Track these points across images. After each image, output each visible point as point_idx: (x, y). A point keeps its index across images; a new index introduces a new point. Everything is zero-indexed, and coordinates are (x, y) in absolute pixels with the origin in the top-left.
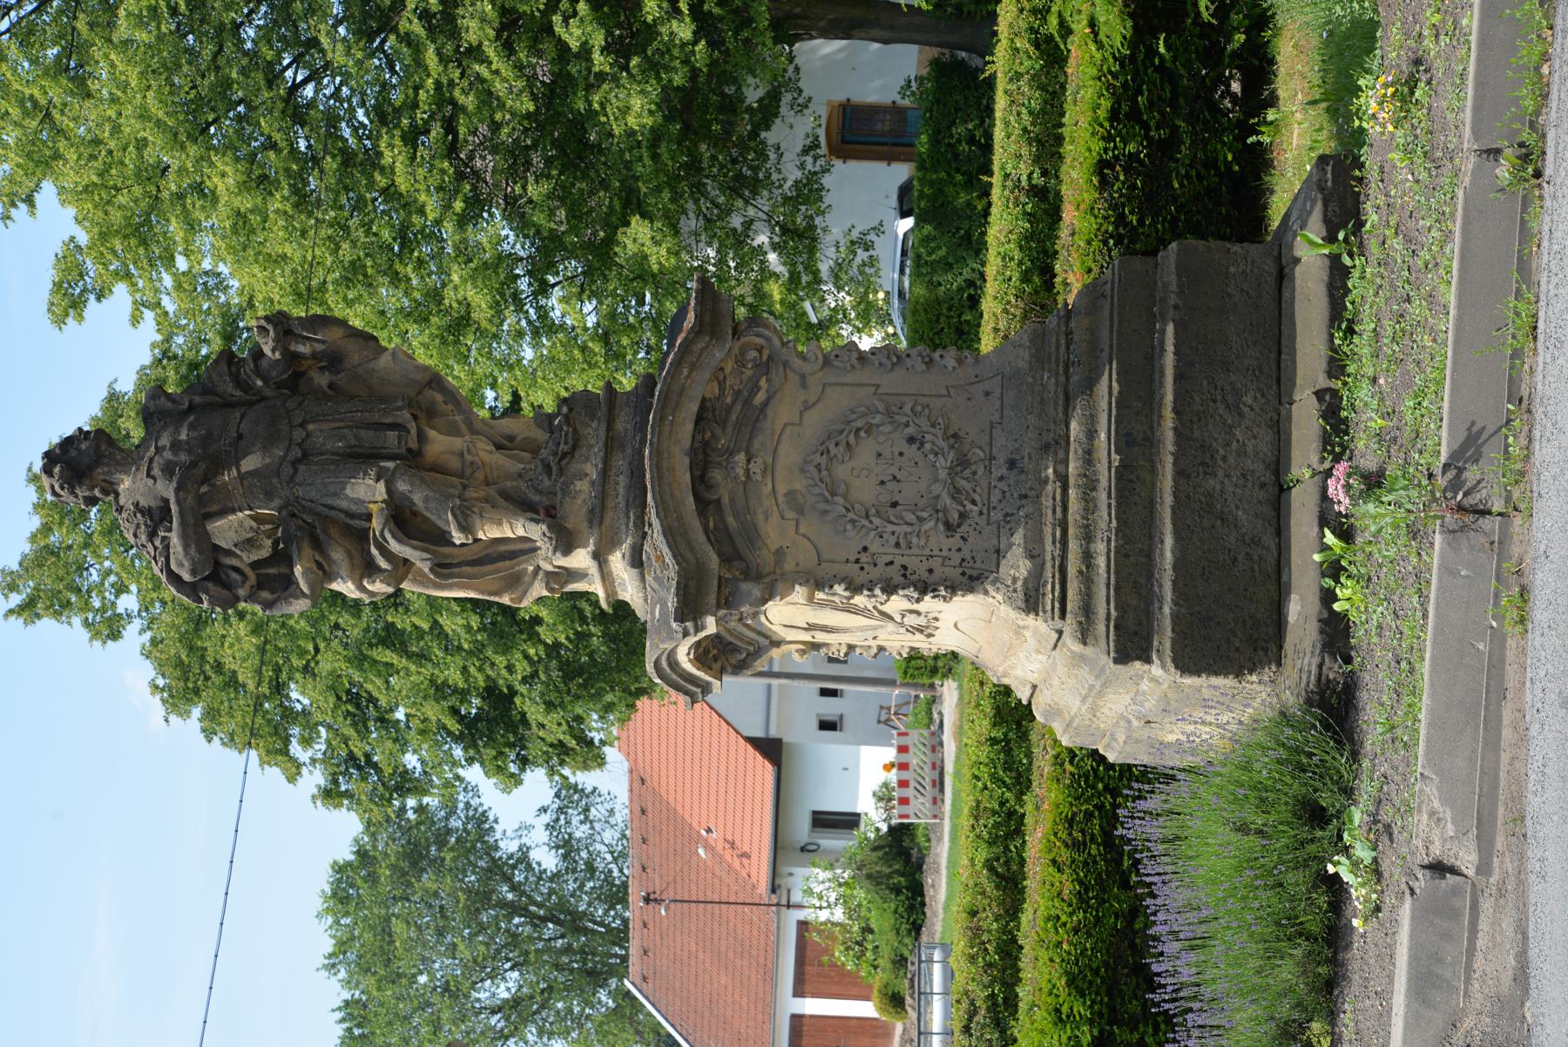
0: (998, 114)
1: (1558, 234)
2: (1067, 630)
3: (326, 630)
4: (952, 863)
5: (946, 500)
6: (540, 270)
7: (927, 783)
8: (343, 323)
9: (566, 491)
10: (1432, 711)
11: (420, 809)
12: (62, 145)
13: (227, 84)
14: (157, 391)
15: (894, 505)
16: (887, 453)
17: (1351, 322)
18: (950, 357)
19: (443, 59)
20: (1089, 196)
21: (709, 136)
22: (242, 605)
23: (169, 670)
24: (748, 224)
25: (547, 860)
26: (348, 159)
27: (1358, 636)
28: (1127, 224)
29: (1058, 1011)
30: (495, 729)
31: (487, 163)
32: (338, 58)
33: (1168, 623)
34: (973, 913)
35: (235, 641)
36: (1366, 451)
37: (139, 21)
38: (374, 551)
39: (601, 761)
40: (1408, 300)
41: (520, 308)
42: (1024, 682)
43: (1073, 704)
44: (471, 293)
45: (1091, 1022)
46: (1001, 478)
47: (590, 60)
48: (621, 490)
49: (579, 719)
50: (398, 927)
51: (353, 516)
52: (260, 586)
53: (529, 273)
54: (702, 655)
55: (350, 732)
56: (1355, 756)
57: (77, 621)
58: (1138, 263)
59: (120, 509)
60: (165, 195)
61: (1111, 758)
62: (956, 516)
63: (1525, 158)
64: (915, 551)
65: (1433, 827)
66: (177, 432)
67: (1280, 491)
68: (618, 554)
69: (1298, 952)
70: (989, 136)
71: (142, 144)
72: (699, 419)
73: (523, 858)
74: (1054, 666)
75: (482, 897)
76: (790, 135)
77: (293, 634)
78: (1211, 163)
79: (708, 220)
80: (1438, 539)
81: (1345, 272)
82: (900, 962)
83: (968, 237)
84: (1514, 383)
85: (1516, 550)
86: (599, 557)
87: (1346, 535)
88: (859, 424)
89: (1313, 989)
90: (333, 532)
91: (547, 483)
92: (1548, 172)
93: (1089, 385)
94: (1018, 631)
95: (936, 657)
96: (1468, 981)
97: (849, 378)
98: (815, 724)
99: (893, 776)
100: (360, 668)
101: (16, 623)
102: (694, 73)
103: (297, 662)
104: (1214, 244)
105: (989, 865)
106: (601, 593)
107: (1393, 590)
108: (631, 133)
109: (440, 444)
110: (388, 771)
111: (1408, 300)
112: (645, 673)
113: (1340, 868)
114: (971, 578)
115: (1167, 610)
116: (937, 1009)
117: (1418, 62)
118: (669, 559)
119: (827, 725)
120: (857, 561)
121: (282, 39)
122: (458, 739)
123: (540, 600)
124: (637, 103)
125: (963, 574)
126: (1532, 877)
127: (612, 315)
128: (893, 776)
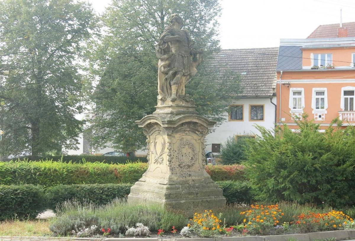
48: (181, 110)
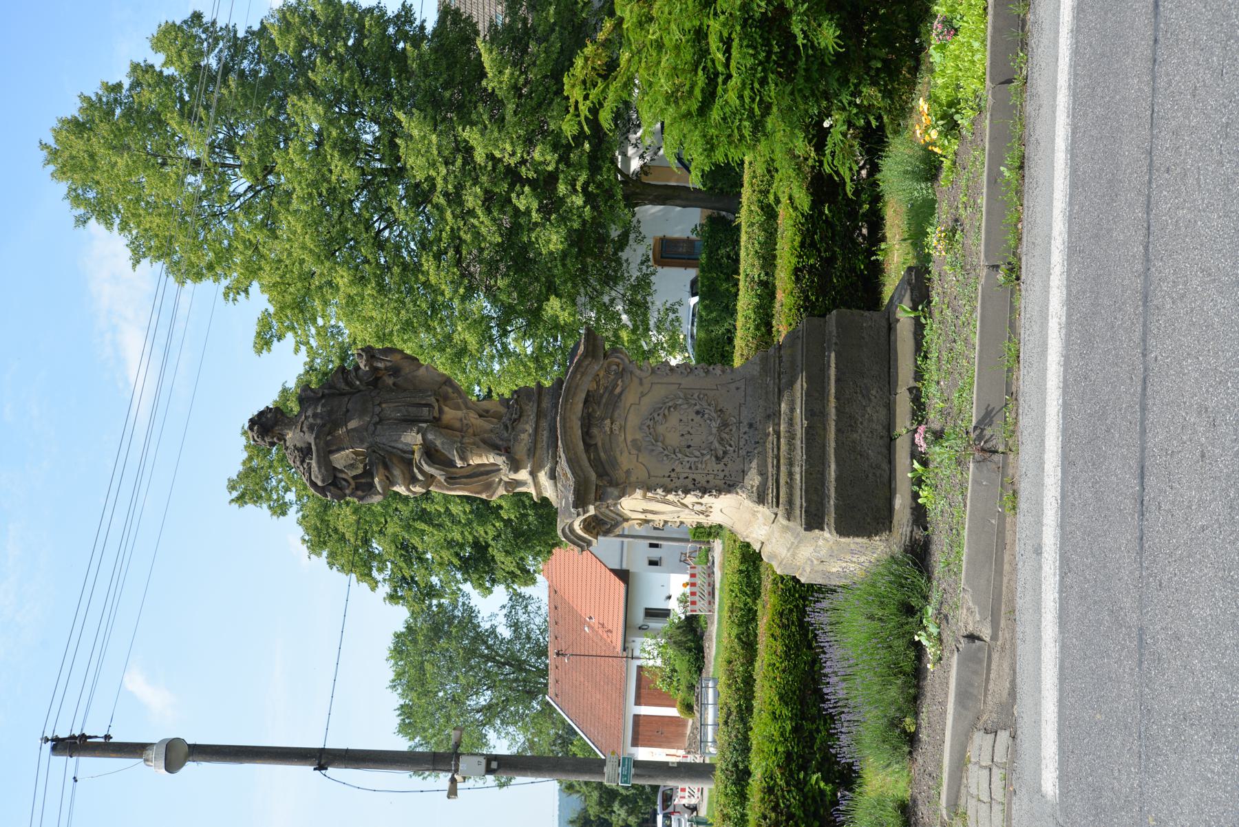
0: (742, 244)
1: (1029, 309)
2: (780, 513)
3: (391, 511)
4: (718, 636)
6: (503, 324)
7: (706, 593)
8: (401, 352)
9: (516, 439)
10: (969, 556)
11: (439, 605)
12: (263, 263)
13: (346, 230)
14: (305, 387)
15: (689, 447)
16: (685, 419)
17: (926, 352)
18: (718, 369)
19: (455, 216)
20: (790, 286)
21: (592, 255)
22: (348, 498)
23: (311, 532)
24: (612, 301)
25: (505, 633)
26: (405, 267)
27: (931, 516)
28: (809, 301)
29: (774, 713)
30: (478, 564)
31: (476, 269)
32: (401, 216)
33: (832, 509)
34: (730, 662)
35: (344, 517)
36: (934, 419)
37: (303, 200)
38: (416, 470)
39: (534, 581)
40: (955, 341)
41: (492, 341)
42: (757, 540)
43: (783, 552)
44: (467, 336)
45: (791, 719)
47: (530, 216)
49: (522, 559)
50: (428, 666)
51: (405, 452)
52: (357, 488)
53: (498, 325)
54: (589, 525)
55: (403, 565)
56: (929, 579)
57: (265, 506)
58: (816, 320)
59: (287, 448)
60: (313, 287)
61: (803, 581)
63: (1011, 270)
65: (969, 616)
66: (316, 408)
67: (891, 440)
68: (543, 472)
69: (899, 682)
70: (738, 255)
71: (302, 262)
72: (586, 401)
73: (493, 631)
74: (773, 532)
75: (472, 652)
76: (634, 255)
77: (374, 514)
78: (853, 270)
79: (591, 298)
80: (971, 465)
81: (923, 327)
82: (691, 687)
83: (727, 307)
84: (1009, 385)
85: (1010, 472)
86: (533, 474)
87: (925, 463)
89: (907, 701)
90: (395, 460)
91: (506, 435)
92: (1023, 277)
93: (791, 384)
94: (754, 513)
95: (711, 527)
96: (985, 696)
97: (665, 380)
98: (647, 562)
99: (688, 590)
100: (408, 531)
101: (235, 506)
102: (584, 222)
103: (375, 528)
104: (855, 311)
105: (738, 637)
106: (534, 494)
107: (946, 490)
108: (551, 253)
109: (450, 414)
110: (422, 585)
111: (955, 341)
112: (556, 535)
113: (921, 638)
115: (832, 503)
116: (711, 711)
117: (956, 220)
118: (570, 475)
119: (653, 563)
121: (374, 208)
122: (459, 569)
123: (502, 497)
124: (554, 238)
126: (1019, 641)
127: (541, 348)
128: (688, 590)
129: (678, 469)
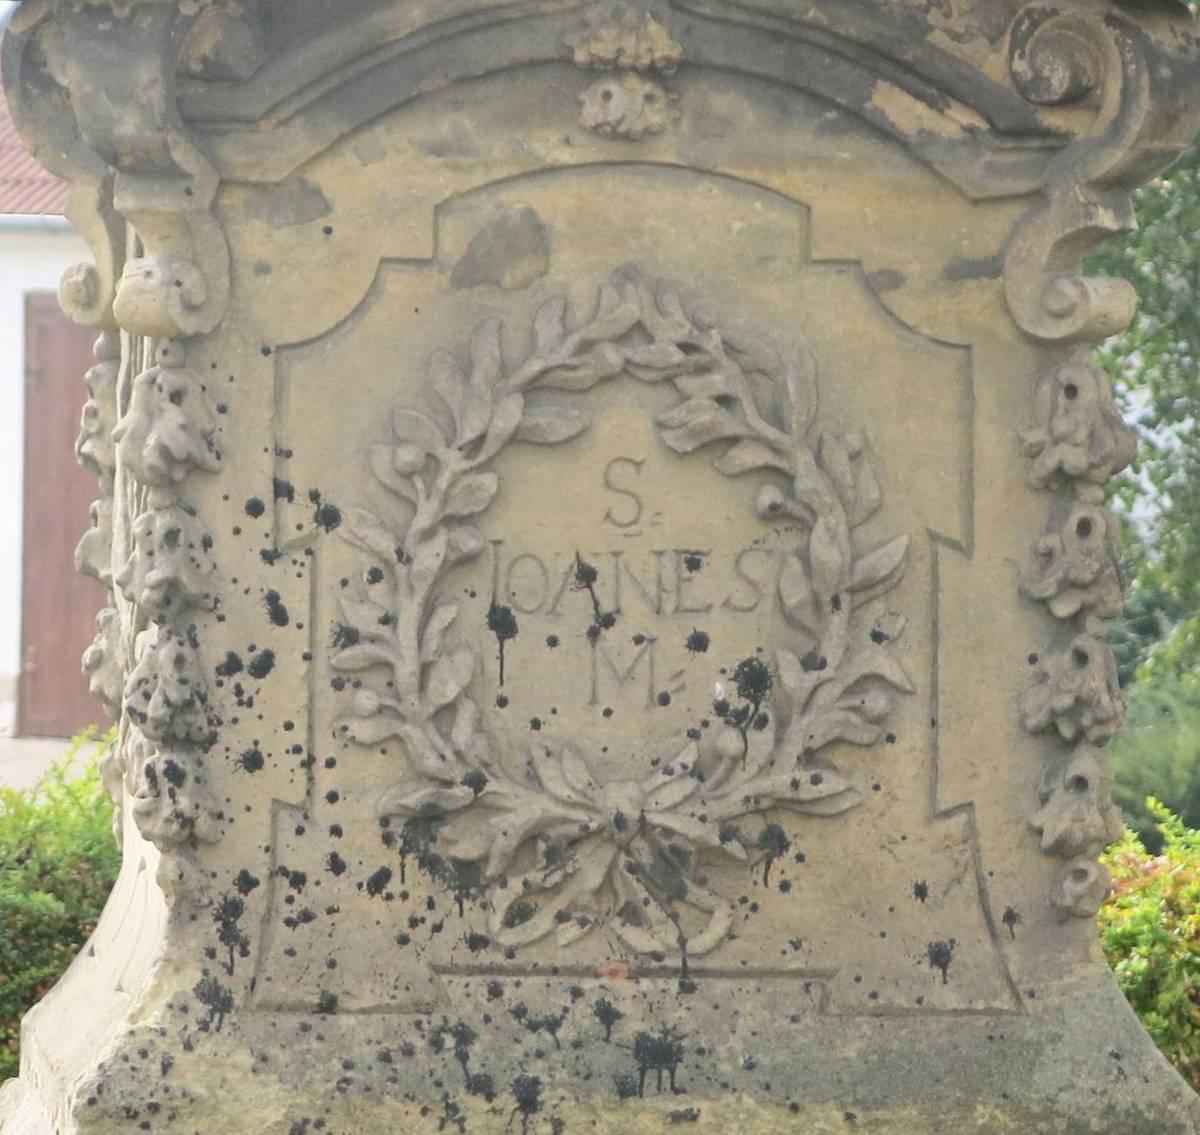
5: (522, 810)
15: (502, 623)
16: (703, 587)
46: (608, 1015)
62: (467, 849)
64: (329, 701)
88: (808, 481)
114: (231, 910)
120: (283, 490)
125: (246, 882)
129: (336, 554)
